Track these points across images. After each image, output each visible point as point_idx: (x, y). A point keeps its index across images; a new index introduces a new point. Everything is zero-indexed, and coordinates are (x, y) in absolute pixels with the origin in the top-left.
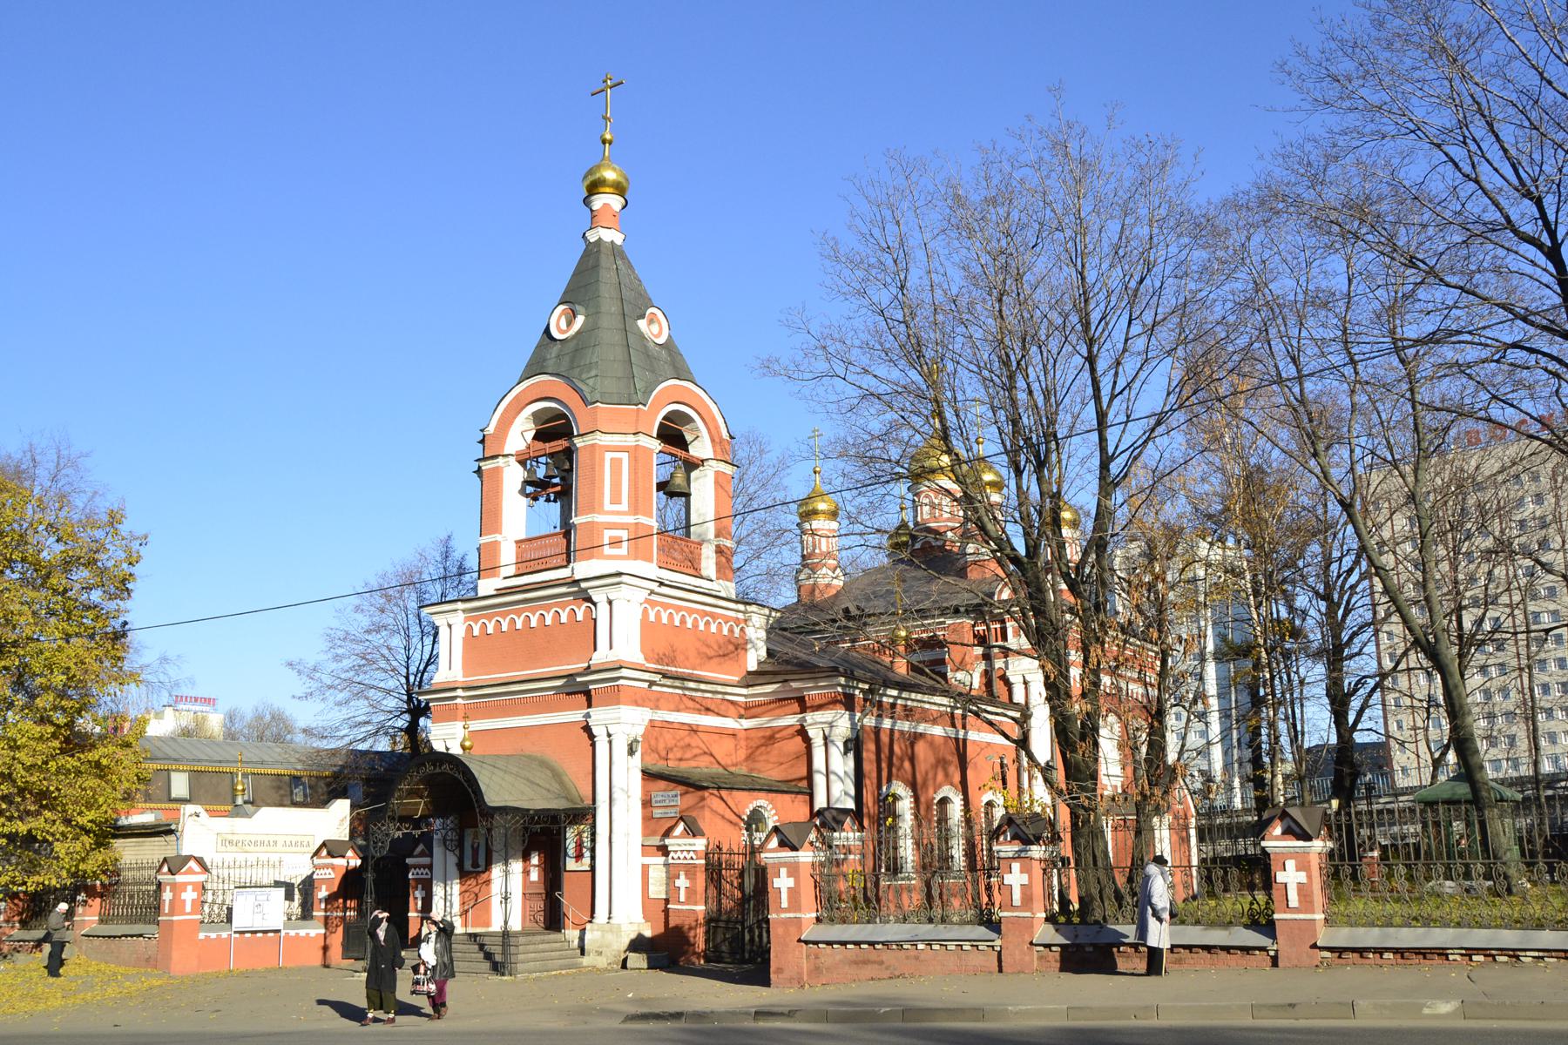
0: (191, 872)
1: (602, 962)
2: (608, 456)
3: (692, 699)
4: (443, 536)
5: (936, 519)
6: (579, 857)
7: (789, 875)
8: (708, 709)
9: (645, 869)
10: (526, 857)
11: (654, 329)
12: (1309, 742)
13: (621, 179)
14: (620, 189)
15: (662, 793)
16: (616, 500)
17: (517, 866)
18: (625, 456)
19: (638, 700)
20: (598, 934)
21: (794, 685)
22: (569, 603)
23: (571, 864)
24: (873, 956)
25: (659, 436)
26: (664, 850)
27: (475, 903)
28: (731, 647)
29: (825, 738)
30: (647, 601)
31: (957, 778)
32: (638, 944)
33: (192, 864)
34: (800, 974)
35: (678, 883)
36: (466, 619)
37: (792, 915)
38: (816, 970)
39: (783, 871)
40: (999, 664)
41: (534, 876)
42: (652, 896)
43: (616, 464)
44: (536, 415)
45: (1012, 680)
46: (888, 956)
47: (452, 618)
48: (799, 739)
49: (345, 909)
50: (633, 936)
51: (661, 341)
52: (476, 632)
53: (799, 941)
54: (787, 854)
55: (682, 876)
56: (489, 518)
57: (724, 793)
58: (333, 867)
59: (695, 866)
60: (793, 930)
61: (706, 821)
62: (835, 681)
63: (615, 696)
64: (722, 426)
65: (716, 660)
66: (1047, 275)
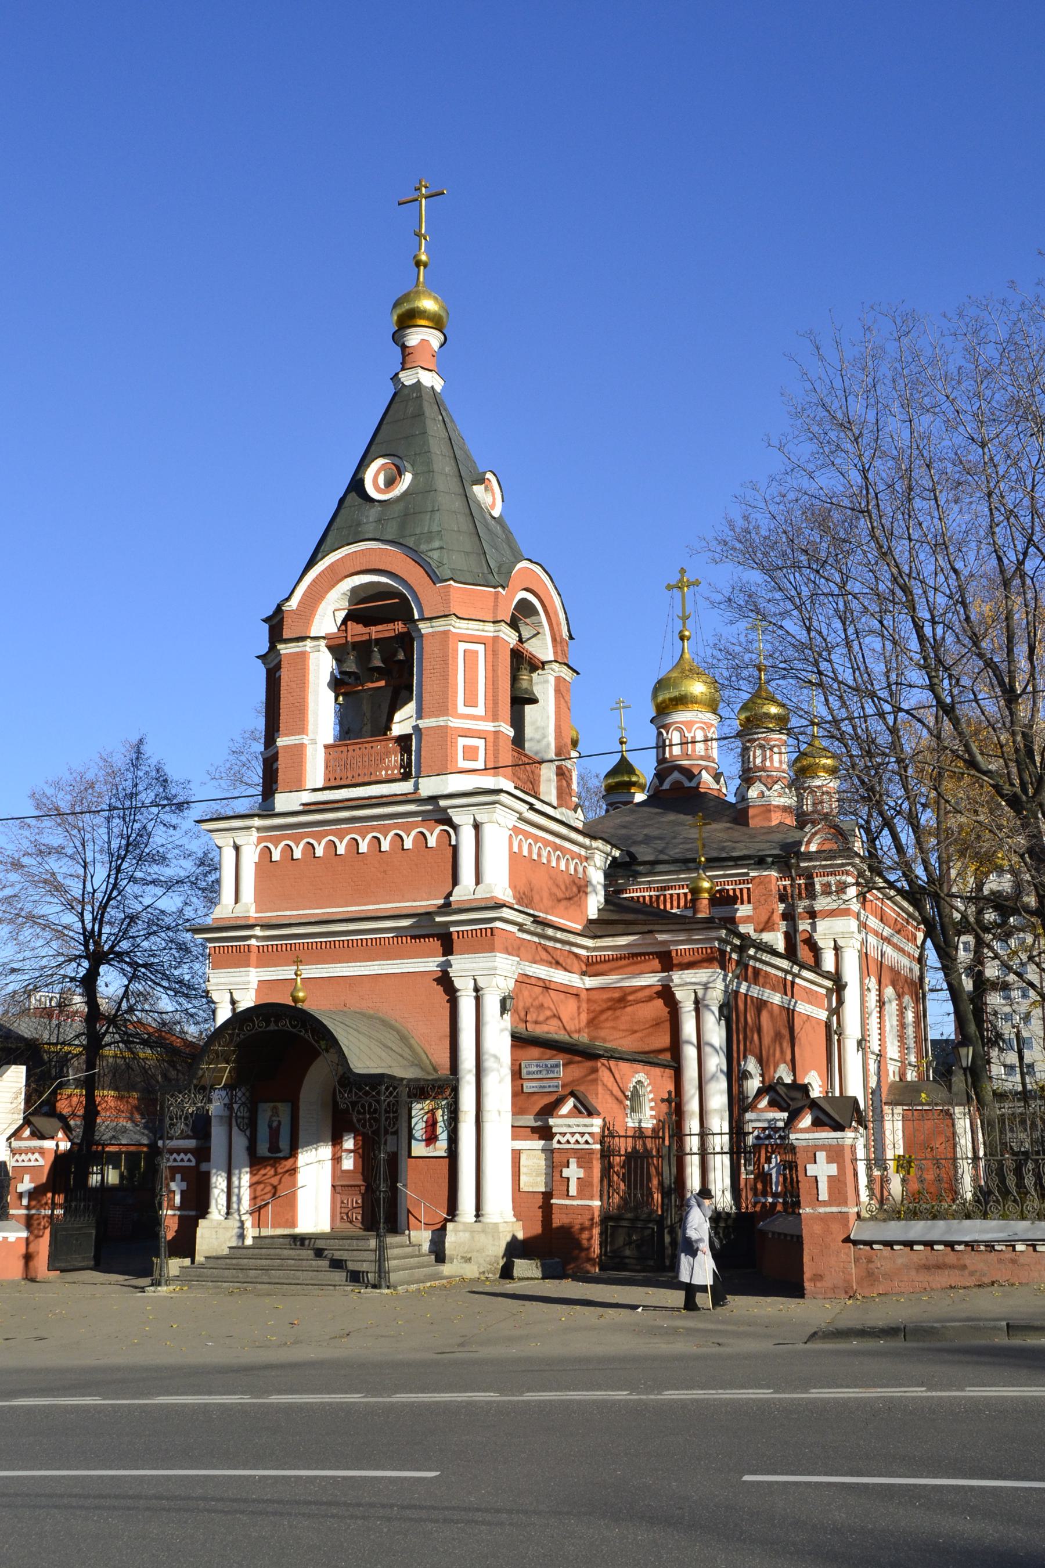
1: (471, 1271)
2: (462, 646)
3: (545, 948)
4: (135, 740)
5: (688, 757)
6: (431, 1139)
7: (830, 1160)
8: (558, 963)
9: (516, 1155)
10: (336, 1141)
12: (933, 1035)
13: (443, 314)
14: (437, 323)
15: (533, 1062)
16: (470, 702)
17: (325, 1151)
19: (514, 949)
20: (464, 1236)
21: (660, 937)
22: (415, 825)
23: (419, 1149)
24: (951, 1258)
26: (545, 1133)
27: (275, 1195)
28: (575, 889)
29: (697, 1002)
30: (515, 829)
31: (789, 1057)
32: (516, 1249)
34: (848, 1282)
36: (260, 840)
37: (834, 1209)
38: (871, 1277)
39: (821, 1156)
40: (804, 925)
41: (348, 1163)
42: (524, 1187)
44: (354, 590)
45: (821, 944)
46: (971, 1260)
47: (241, 839)
48: (659, 1003)
49: (54, 1206)
50: (509, 1238)
53: (847, 1240)
54: (826, 1135)
55: (573, 1162)
57: (612, 1063)
58: (42, 1151)
59: (591, 1152)
60: (835, 1227)
61: (600, 1100)
62: (714, 934)
63: (486, 940)
64: (563, 622)
65: (564, 903)
66: (920, 474)
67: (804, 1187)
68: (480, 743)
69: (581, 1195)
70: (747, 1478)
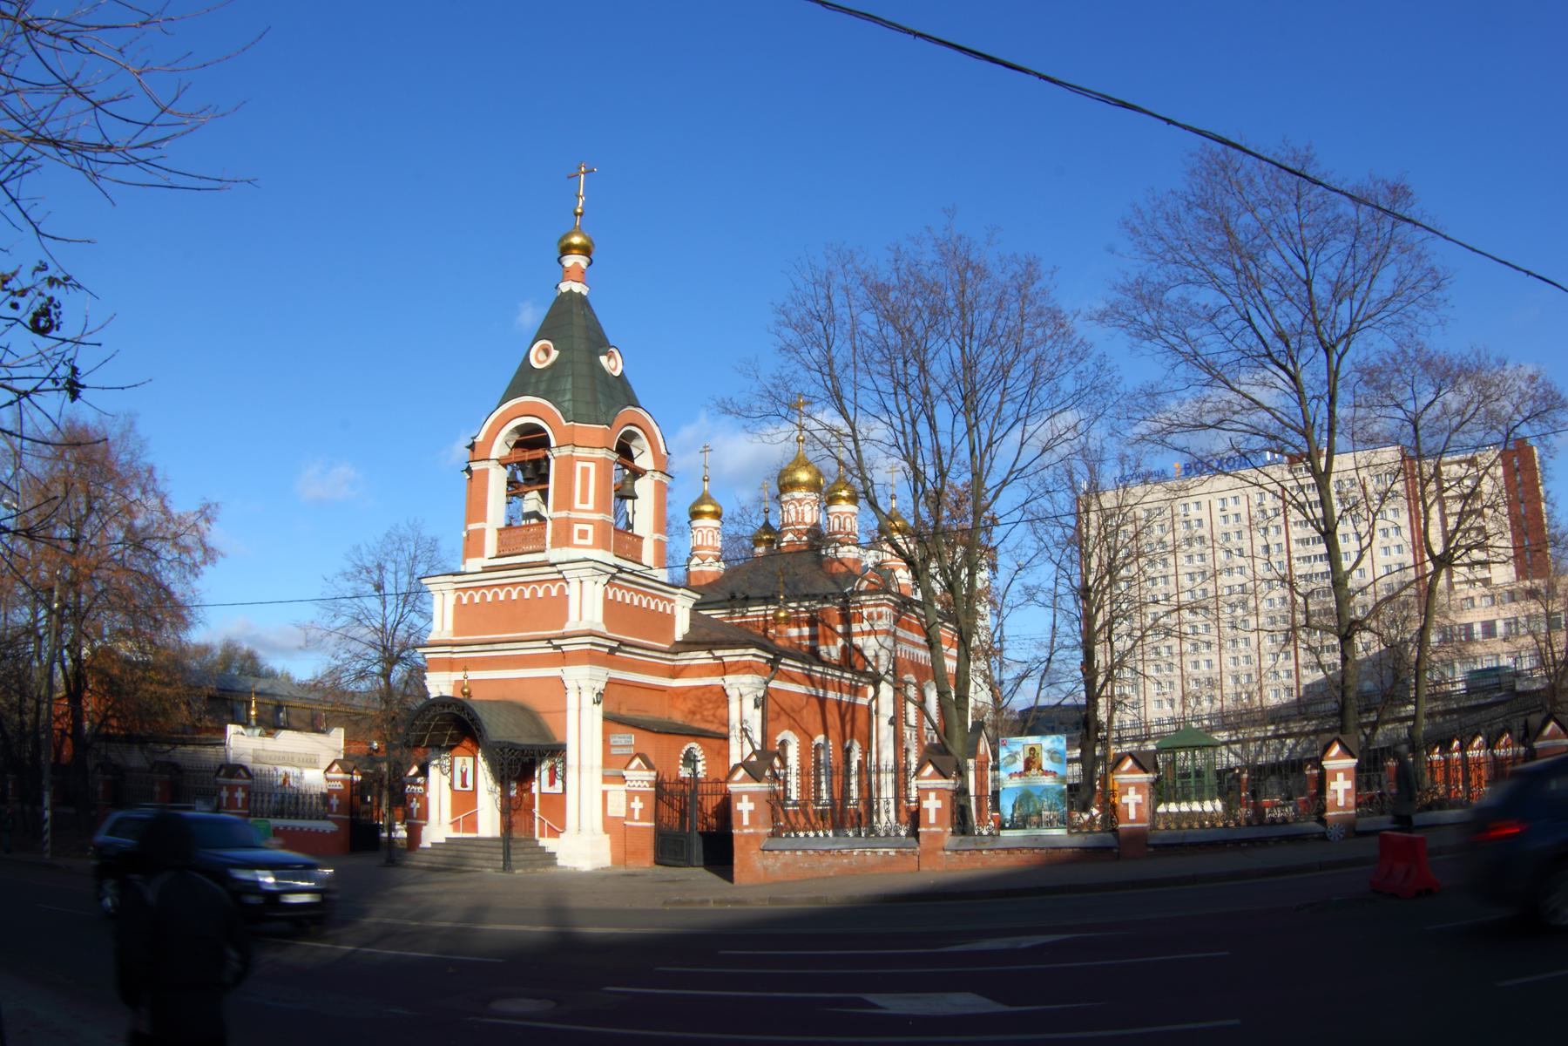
0: (240, 776)
9: (605, 794)
11: (612, 365)
14: (585, 250)
16: (584, 500)
18: (592, 466)
25: (618, 451)
33: (242, 773)
35: (633, 805)
39: (745, 798)
43: (585, 471)
44: (519, 429)
51: (617, 373)
52: (465, 601)
56: (477, 509)
67: (734, 817)
68: (590, 528)
69: (641, 819)
70: (1237, 1021)
